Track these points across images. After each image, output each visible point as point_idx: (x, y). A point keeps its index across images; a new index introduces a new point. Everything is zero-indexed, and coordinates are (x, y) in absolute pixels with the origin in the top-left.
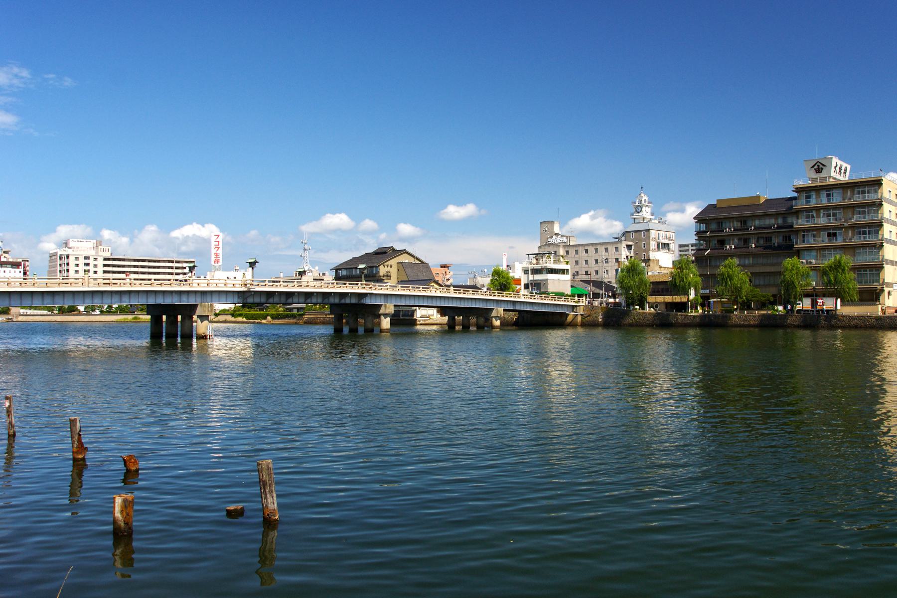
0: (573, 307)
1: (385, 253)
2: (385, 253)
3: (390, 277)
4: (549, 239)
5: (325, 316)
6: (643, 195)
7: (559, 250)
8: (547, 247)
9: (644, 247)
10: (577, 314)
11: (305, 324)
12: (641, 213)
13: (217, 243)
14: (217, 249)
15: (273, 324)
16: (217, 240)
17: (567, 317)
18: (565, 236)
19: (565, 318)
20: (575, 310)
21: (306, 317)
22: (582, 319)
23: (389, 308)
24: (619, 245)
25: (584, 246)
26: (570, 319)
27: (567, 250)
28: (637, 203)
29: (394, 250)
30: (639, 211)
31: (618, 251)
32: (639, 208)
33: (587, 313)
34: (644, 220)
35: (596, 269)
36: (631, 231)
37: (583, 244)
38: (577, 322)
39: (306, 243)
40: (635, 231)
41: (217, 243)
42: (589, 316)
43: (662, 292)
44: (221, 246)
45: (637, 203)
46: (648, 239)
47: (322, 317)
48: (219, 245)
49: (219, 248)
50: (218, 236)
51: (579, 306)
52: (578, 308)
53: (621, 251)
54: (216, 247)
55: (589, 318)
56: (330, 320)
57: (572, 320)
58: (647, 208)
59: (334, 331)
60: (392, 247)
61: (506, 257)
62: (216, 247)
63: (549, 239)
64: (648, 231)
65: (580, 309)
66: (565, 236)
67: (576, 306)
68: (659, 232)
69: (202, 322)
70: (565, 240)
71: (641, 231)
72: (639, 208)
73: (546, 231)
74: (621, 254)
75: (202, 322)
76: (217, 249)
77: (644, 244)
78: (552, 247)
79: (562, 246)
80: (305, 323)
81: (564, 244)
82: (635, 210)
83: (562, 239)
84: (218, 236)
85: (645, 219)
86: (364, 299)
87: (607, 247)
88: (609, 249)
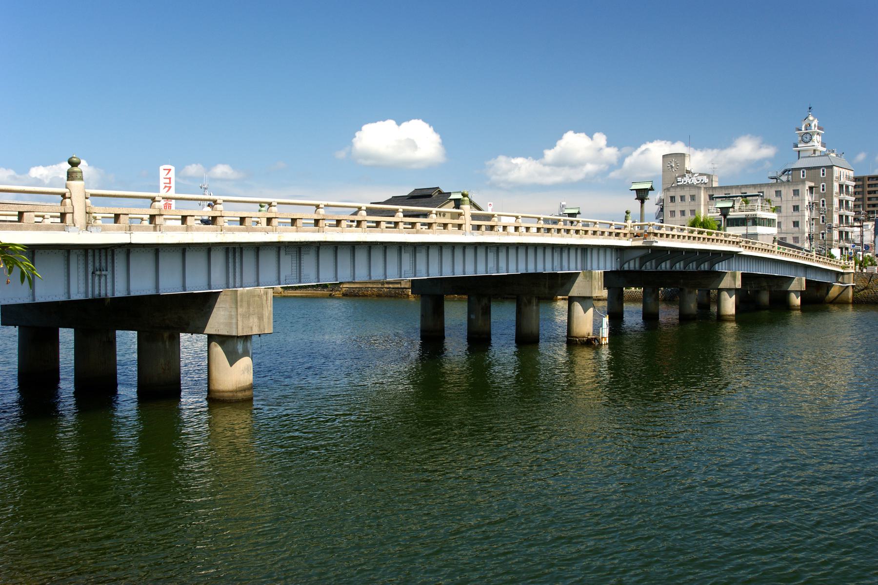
0: (838, 274)
1: (430, 196)
2: (430, 196)
3: (297, 232)
4: (679, 179)
5: (380, 286)
6: (811, 118)
7: (699, 194)
8: (679, 189)
9: (823, 190)
10: (848, 286)
11: (344, 297)
12: (811, 144)
13: (168, 181)
14: (167, 189)
15: (284, 296)
16: (168, 176)
17: (828, 291)
18: (705, 175)
19: (825, 292)
20: (840, 280)
21: (345, 286)
22: (854, 292)
23: (799, 283)
24: (799, 187)
25: (740, 188)
26: (834, 292)
27: (711, 193)
28: (803, 129)
29: (440, 192)
30: (808, 140)
31: (798, 195)
32: (808, 136)
33: (862, 285)
34: (814, 153)
35: (795, 219)
36: (802, 168)
37: (738, 186)
38: (848, 298)
39: (206, 189)
40: (808, 169)
41: (168, 181)
42: (866, 288)
43: (234, 249)
44: (173, 184)
45: (803, 129)
46: (830, 179)
47: (375, 286)
48: (170, 183)
49: (170, 187)
50: (170, 170)
51: (849, 273)
52: (846, 276)
53: (803, 196)
54: (166, 187)
55: (866, 291)
56: (390, 291)
57: (839, 295)
58: (818, 136)
59: (643, 319)
60: (438, 188)
61: (492, 207)
62: (166, 187)
63: (679, 179)
64: (831, 167)
65: (849, 278)
66: (705, 175)
67: (843, 274)
68: (841, 169)
69: (585, 312)
70: (706, 180)
71: (819, 168)
72: (808, 136)
73: (672, 167)
74: (803, 200)
75: (585, 312)
76: (167, 189)
77: (823, 186)
78: (687, 189)
79: (703, 189)
80: (345, 295)
81: (704, 186)
82: (800, 138)
83: (700, 178)
84: (170, 170)
85: (816, 152)
86: (717, 265)
87: (779, 189)
88: (783, 193)
